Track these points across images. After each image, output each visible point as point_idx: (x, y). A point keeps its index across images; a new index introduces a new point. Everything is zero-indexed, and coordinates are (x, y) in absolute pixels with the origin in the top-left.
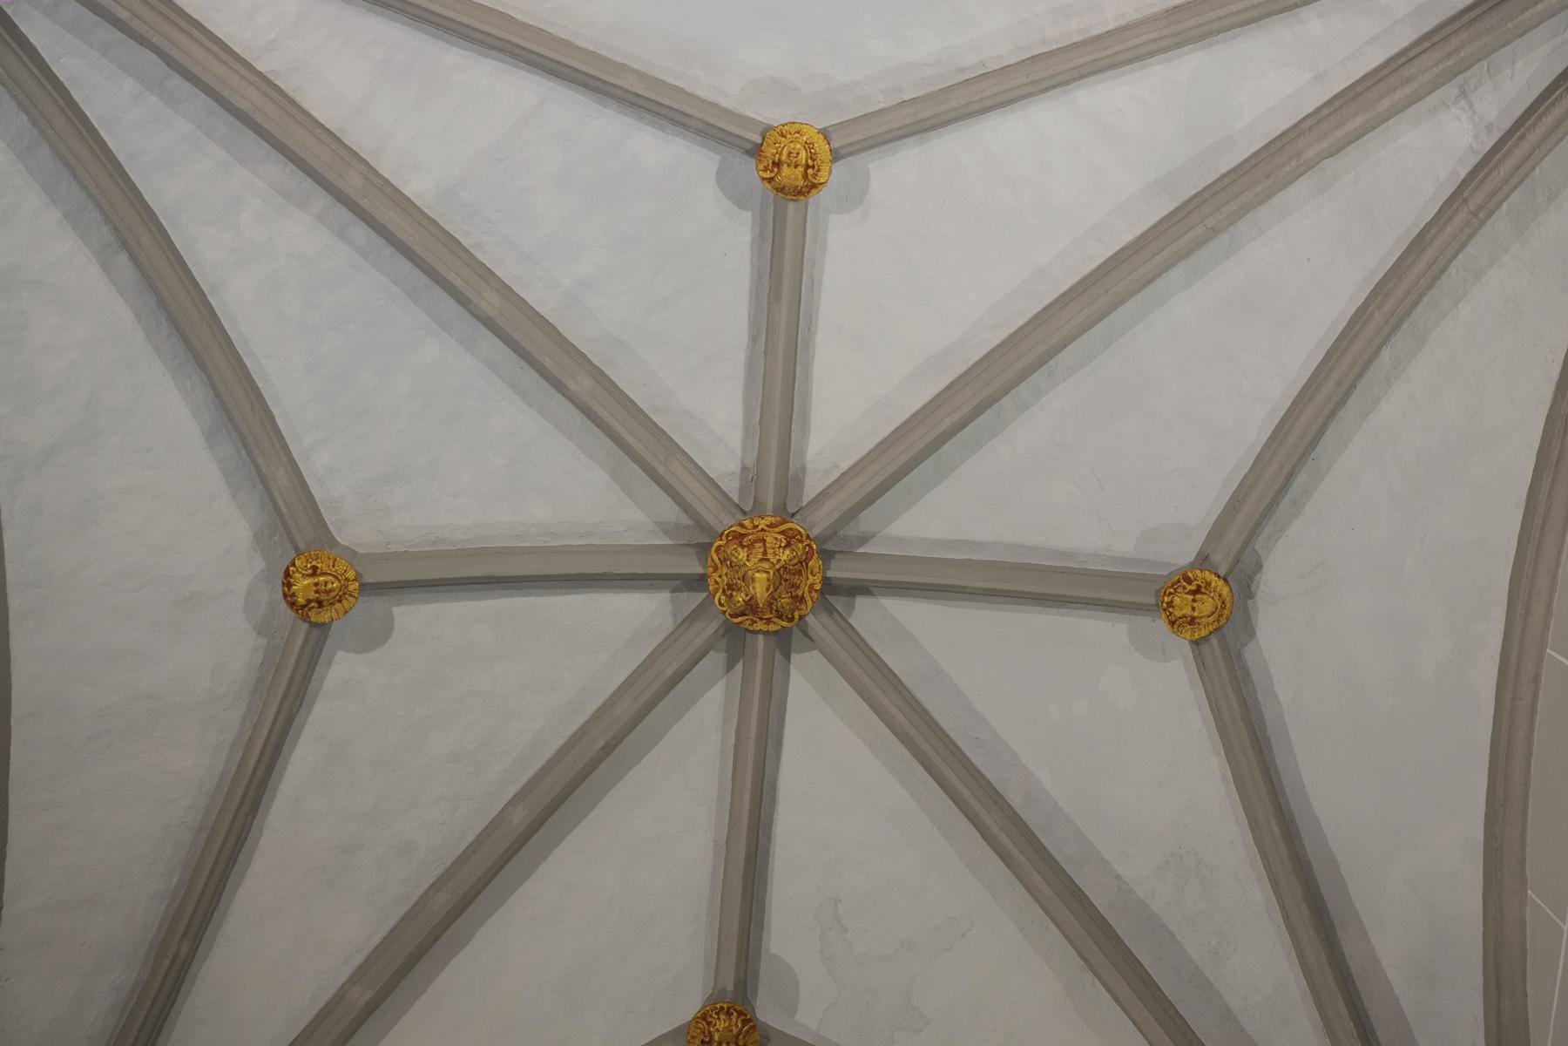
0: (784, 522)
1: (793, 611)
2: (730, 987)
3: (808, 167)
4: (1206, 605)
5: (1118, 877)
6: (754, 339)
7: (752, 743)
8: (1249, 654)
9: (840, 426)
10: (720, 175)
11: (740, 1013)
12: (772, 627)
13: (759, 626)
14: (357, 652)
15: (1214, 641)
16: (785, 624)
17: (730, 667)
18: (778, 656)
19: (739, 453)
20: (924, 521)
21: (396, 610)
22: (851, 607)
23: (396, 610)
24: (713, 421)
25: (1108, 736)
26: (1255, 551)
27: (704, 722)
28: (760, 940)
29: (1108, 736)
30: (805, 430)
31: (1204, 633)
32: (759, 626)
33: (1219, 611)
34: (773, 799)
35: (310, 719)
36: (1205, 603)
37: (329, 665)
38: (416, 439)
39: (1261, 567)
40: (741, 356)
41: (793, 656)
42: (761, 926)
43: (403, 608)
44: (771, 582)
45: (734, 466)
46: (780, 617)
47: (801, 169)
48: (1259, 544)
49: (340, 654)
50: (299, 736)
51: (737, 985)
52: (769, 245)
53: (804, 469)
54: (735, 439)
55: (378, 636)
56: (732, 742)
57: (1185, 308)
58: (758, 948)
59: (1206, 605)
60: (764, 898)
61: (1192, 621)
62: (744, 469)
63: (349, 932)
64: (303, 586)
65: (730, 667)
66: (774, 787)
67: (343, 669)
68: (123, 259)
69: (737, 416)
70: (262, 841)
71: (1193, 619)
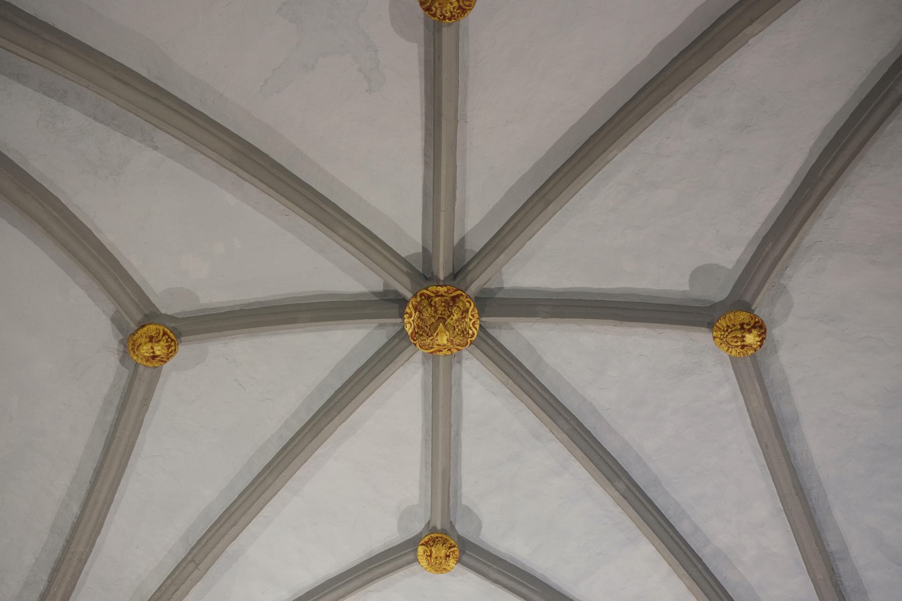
0: (432, 353)
1: (421, 300)
2: (445, 30)
3: (430, 556)
4: (145, 350)
5: (156, 148)
6: (458, 434)
7: (443, 208)
8: (111, 308)
9: (404, 391)
10: (480, 526)
11: (434, 15)
12: (433, 288)
13: (442, 290)
14: (718, 266)
15: (134, 327)
16: (425, 291)
17: (463, 240)
18: (430, 250)
19: (463, 370)
20: (344, 344)
21: (687, 288)
22: (385, 284)
23: (687, 288)
24: (479, 387)
25: (190, 234)
26: (127, 368)
27: (479, 206)
28: (426, 52)
29: (190, 234)
30: (424, 384)
31: (142, 331)
32: (442, 290)
33: (136, 347)
34: (426, 155)
35: (759, 226)
36: (153, 332)
37: (738, 261)
38: (663, 393)
39: (120, 361)
40: (465, 425)
41: (420, 250)
42: (426, 61)
43: (682, 289)
44: (440, 298)
45: (466, 363)
46: (429, 297)
47: (434, 556)
48: (126, 373)
49: (730, 267)
50: (769, 216)
51: (440, 30)
52: (452, 485)
53: (423, 363)
54: (466, 378)
55: (700, 273)
56: (458, 192)
57: (209, 494)
58: (427, 45)
59: (145, 350)
60: (426, 84)
61: (151, 339)
62: (460, 362)
63: (757, 62)
64: (751, 338)
65: (463, 240)
66: (426, 163)
67: (730, 254)
68: (833, 546)
69: (465, 391)
70: (812, 143)
71: (151, 341)
